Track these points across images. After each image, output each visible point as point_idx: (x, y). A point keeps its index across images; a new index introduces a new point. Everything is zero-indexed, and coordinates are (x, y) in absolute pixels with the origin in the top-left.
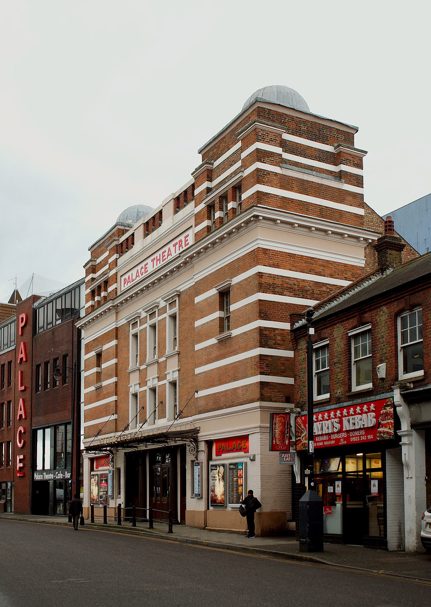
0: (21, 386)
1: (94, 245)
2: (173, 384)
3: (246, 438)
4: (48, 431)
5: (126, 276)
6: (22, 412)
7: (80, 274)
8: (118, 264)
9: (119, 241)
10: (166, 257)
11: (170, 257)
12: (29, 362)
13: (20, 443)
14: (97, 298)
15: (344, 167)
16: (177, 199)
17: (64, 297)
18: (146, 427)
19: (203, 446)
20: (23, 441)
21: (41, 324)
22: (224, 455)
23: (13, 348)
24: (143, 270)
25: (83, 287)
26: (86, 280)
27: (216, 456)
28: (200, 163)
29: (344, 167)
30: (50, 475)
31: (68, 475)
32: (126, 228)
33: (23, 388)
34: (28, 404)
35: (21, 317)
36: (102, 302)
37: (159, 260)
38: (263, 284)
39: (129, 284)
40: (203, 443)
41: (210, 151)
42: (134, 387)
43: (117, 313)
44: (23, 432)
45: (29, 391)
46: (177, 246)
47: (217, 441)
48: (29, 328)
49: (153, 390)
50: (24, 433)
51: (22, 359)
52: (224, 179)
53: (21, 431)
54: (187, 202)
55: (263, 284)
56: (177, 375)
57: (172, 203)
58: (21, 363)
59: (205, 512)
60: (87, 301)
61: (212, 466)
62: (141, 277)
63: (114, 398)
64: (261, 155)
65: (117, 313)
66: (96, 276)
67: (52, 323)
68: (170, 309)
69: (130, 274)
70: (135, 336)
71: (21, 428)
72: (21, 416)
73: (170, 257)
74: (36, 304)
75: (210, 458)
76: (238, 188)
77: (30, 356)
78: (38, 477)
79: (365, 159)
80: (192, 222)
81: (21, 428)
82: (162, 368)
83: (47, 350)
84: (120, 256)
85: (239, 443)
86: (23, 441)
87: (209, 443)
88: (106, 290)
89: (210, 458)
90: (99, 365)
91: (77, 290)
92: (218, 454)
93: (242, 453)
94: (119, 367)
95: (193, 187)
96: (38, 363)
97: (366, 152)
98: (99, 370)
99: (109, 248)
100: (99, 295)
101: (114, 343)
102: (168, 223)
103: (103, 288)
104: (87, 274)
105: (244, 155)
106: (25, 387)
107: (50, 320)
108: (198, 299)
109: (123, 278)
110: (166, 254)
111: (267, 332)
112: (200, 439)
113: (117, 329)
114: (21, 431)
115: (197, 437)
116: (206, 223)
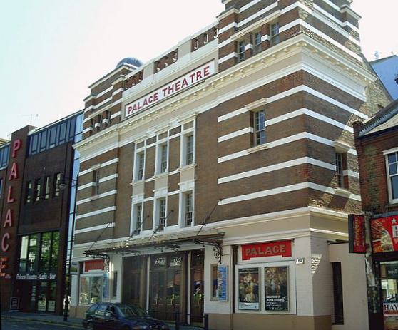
0: (10, 198)
1: (96, 83)
3: (288, 243)
5: (132, 105)
6: (9, 221)
7: (81, 106)
8: (123, 96)
9: (126, 75)
10: (181, 86)
11: (145, 106)
12: (20, 179)
13: (5, 247)
16: (194, 40)
17: (69, 122)
19: (227, 251)
20: (8, 246)
21: (34, 148)
22: (90, 271)
23: (5, 168)
24: (152, 99)
25: (79, 118)
26: (86, 111)
27: (243, 260)
28: (89, 94)
30: (34, 276)
31: (52, 277)
32: (130, 69)
33: (12, 201)
34: (16, 214)
35: (16, 142)
36: (239, 59)
37: (173, 89)
39: (135, 111)
40: (230, 247)
41: (96, 89)
42: (138, 198)
44: (8, 237)
45: (17, 203)
46: (195, 77)
47: (244, 246)
48: (22, 152)
49: (162, 201)
50: (10, 238)
51: (13, 176)
52: (101, 108)
53: (6, 237)
54: (211, 39)
56: (194, 186)
57: (153, 65)
58: (11, 180)
59: (232, 316)
60: (84, 128)
61: (240, 270)
62: (149, 104)
63: (113, 208)
67: (36, 150)
68: (159, 139)
69: (136, 103)
70: (141, 155)
71: (7, 235)
72: (8, 224)
73: (145, 106)
75: (235, 262)
77: (21, 174)
78: (20, 277)
79: (360, 21)
80: (216, 56)
81: (7, 235)
82: (173, 183)
83: (38, 170)
84: (125, 90)
85: (284, 247)
86: (8, 246)
87: (235, 248)
89: (235, 262)
91: (73, 120)
92: (86, 270)
93: (100, 271)
94: (120, 182)
95: (214, 29)
96: (28, 180)
97: (360, 17)
98: (95, 184)
99: (113, 84)
101: (116, 160)
102: (148, 81)
104: (87, 105)
105: (114, 94)
106: (14, 200)
107: (43, 145)
108: (221, 119)
109: (127, 107)
110: (181, 84)
111: (310, 144)
113: (118, 148)
114: (6, 237)
115: (222, 242)
116: (89, 129)
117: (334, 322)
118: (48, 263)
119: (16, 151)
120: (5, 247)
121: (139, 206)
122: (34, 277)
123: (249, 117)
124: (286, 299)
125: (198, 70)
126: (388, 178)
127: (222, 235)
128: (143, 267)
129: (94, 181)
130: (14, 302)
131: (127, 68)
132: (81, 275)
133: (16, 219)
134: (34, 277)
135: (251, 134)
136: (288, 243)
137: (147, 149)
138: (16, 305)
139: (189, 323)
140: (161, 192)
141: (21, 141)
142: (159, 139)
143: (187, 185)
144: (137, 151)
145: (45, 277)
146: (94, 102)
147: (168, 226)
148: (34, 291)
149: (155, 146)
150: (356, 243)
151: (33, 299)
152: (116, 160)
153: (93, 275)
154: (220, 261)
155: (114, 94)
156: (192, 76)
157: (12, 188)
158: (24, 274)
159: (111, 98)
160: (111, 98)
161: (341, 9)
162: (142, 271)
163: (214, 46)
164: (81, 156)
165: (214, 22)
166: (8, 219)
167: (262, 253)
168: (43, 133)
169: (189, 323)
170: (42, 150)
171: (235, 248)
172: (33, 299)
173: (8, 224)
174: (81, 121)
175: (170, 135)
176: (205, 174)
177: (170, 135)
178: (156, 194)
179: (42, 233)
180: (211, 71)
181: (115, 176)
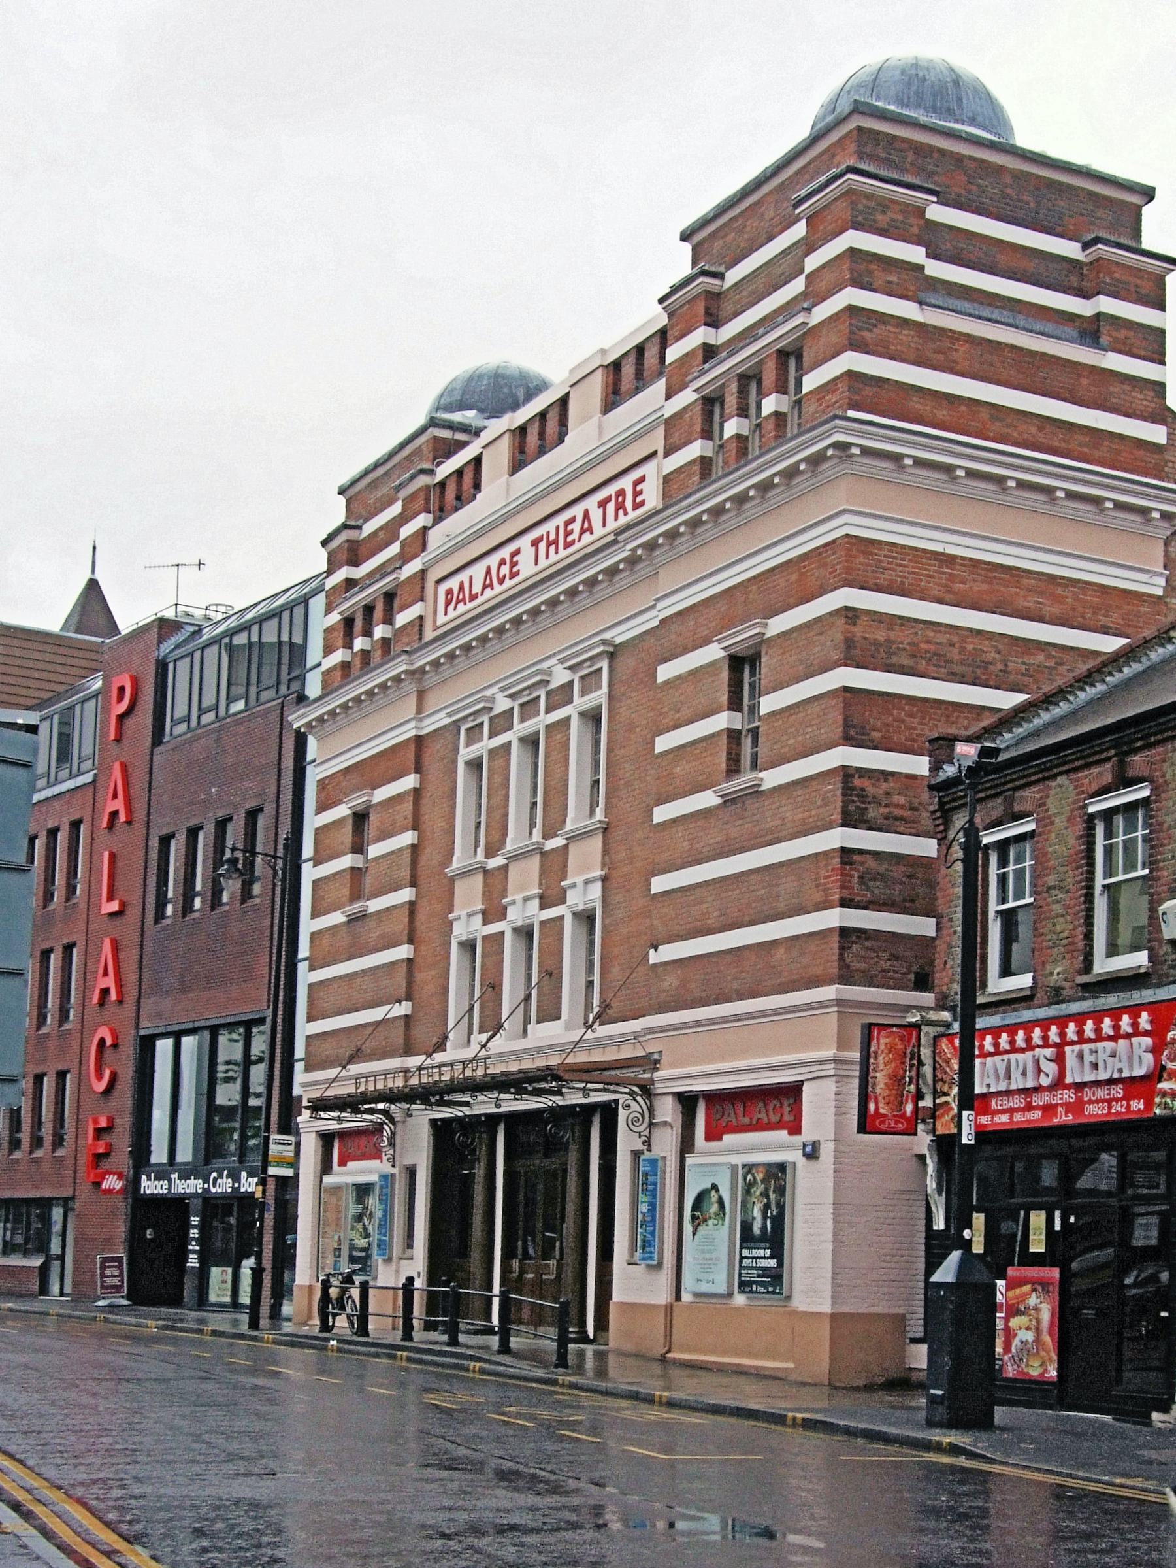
2: (586, 918)
3: (794, 1091)
4: (188, 1042)
5: (453, 583)
7: (319, 561)
10: (575, 536)
14: (359, 643)
15: (1106, 304)
18: (499, 1044)
19: (667, 1110)
21: (181, 710)
23: (88, 778)
24: (505, 570)
25: (318, 604)
26: (330, 583)
29: (1106, 304)
33: (114, 906)
36: (377, 656)
37: (556, 542)
38: (860, 640)
42: (467, 925)
43: (421, 695)
45: (134, 913)
47: (714, 1098)
49: (525, 933)
50: (115, 1046)
51: (114, 815)
53: (102, 1041)
54: (641, 381)
55: (860, 640)
60: (328, 650)
63: (403, 952)
64: (862, 269)
65: (421, 695)
66: (358, 573)
67: (216, 708)
69: (463, 576)
70: (475, 765)
74: (166, 647)
76: (791, 357)
78: (150, 1187)
80: (657, 441)
85: (778, 1103)
87: (687, 1102)
88: (388, 620)
90: (358, 848)
91: (299, 611)
92: (342, 1163)
96: (165, 831)
100: (368, 633)
101: (410, 782)
103: (378, 613)
106: (123, 905)
110: (576, 527)
112: (660, 1088)
113: (419, 740)
114: (102, 1041)
116: (695, 449)
117: (920, 1333)
118: (236, 1136)
119: (121, 718)
120: (100, 1077)
121: (469, 946)
122: (194, 1185)
123: (725, 675)
124: (780, 1264)
125: (512, 547)
126: (1098, 889)
127: (651, 1063)
128: (483, 1152)
129: (735, 704)
130: (108, 1272)
131: (446, 434)
132: (327, 1179)
133: (130, 977)
134: (194, 1185)
135: (733, 736)
136: (794, 1091)
137: (492, 752)
138: (116, 1282)
139: (591, 1334)
140: (523, 909)
141: (135, 682)
142: (522, 720)
143: (583, 892)
144: (466, 753)
145: (224, 1185)
146: (354, 554)
147: (538, 1022)
148: (194, 1233)
149: (569, 718)
150: (879, 1106)
151: (193, 1262)
152: (410, 782)
153: (739, 1160)
154: (648, 1143)
155: (812, 262)
156: (603, 504)
157: (113, 856)
158: (162, 1174)
159: (797, 286)
160: (797, 286)
161: (1086, 246)
162: (480, 1171)
163: (651, 402)
164: (325, 760)
165: (648, 316)
166: (106, 974)
167: (746, 1120)
168: (207, 652)
169: (591, 1334)
170: (208, 718)
171: (687, 1102)
172: (193, 1262)
173: (105, 992)
174: (322, 620)
175: (547, 712)
176: (629, 848)
177: (547, 712)
178: (570, 901)
179: (214, 1031)
180: (652, 496)
181: (408, 838)
